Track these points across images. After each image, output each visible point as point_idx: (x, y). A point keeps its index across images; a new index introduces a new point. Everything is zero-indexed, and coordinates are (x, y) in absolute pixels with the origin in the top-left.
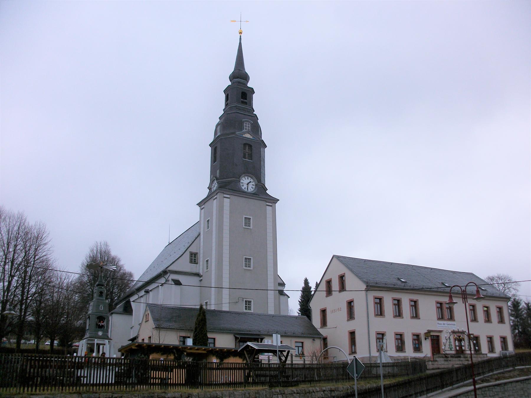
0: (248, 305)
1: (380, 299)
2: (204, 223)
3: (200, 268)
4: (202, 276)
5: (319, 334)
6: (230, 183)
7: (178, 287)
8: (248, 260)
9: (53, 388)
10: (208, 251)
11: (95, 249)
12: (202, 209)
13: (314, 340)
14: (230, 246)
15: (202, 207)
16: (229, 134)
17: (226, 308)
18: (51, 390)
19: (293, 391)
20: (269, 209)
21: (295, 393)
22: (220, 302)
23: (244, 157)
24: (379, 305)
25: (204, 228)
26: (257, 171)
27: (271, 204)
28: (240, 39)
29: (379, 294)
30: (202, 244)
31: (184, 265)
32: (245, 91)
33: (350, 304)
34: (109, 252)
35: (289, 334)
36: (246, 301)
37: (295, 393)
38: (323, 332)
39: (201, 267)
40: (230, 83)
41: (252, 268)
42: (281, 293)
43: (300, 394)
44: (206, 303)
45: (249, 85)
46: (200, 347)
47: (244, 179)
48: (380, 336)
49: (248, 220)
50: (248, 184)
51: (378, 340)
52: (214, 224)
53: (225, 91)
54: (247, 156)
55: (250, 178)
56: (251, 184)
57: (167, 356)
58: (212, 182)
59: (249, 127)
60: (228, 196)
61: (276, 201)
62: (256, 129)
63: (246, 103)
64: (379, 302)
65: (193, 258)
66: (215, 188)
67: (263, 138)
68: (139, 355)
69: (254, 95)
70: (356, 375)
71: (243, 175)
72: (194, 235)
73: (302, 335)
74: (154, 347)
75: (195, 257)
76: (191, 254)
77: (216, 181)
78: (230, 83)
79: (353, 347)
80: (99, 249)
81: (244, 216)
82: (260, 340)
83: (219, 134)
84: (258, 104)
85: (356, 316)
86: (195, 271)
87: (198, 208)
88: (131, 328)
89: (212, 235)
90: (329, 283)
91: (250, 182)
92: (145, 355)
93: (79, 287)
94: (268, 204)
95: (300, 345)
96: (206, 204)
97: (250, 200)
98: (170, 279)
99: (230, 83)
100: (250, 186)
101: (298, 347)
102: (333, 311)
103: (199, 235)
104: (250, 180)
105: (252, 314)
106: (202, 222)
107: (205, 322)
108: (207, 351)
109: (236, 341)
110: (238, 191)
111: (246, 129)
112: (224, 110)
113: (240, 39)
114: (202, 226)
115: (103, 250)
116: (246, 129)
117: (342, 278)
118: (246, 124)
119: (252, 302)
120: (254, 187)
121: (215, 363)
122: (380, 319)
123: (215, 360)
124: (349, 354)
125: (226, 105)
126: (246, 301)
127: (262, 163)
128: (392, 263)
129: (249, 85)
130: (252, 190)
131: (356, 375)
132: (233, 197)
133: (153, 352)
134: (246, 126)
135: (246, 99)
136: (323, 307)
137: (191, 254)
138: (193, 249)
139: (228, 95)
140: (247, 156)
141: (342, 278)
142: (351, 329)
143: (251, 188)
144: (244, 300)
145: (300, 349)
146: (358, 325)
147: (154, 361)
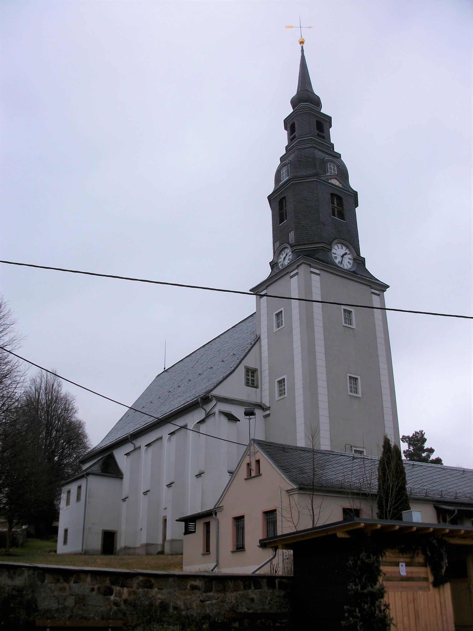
2: (269, 320)
3: (265, 393)
4: (269, 408)
6: (316, 250)
14: (327, 354)
23: (334, 215)
27: (377, 292)
28: (302, 51)
31: (235, 387)
32: (321, 121)
39: (266, 393)
41: (360, 395)
47: (336, 247)
50: (342, 257)
54: (336, 213)
55: (344, 248)
58: (277, 252)
60: (317, 271)
61: (384, 287)
62: (343, 174)
65: (250, 378)
66: (287, 262)
71: (336, 241)
75: (253, 376)
84: (340, 138)
91: (346, 254)
98: (216, 410)
103: (258, 339)
110: (328, 265)
112: (287, 148)
113: (302, 51)
120: (351, 262)
125: (291, 139)
130: (350, 266)
134: (331, 168)
138: (250, 362)
140: (336, 213)
144: (354, 449)
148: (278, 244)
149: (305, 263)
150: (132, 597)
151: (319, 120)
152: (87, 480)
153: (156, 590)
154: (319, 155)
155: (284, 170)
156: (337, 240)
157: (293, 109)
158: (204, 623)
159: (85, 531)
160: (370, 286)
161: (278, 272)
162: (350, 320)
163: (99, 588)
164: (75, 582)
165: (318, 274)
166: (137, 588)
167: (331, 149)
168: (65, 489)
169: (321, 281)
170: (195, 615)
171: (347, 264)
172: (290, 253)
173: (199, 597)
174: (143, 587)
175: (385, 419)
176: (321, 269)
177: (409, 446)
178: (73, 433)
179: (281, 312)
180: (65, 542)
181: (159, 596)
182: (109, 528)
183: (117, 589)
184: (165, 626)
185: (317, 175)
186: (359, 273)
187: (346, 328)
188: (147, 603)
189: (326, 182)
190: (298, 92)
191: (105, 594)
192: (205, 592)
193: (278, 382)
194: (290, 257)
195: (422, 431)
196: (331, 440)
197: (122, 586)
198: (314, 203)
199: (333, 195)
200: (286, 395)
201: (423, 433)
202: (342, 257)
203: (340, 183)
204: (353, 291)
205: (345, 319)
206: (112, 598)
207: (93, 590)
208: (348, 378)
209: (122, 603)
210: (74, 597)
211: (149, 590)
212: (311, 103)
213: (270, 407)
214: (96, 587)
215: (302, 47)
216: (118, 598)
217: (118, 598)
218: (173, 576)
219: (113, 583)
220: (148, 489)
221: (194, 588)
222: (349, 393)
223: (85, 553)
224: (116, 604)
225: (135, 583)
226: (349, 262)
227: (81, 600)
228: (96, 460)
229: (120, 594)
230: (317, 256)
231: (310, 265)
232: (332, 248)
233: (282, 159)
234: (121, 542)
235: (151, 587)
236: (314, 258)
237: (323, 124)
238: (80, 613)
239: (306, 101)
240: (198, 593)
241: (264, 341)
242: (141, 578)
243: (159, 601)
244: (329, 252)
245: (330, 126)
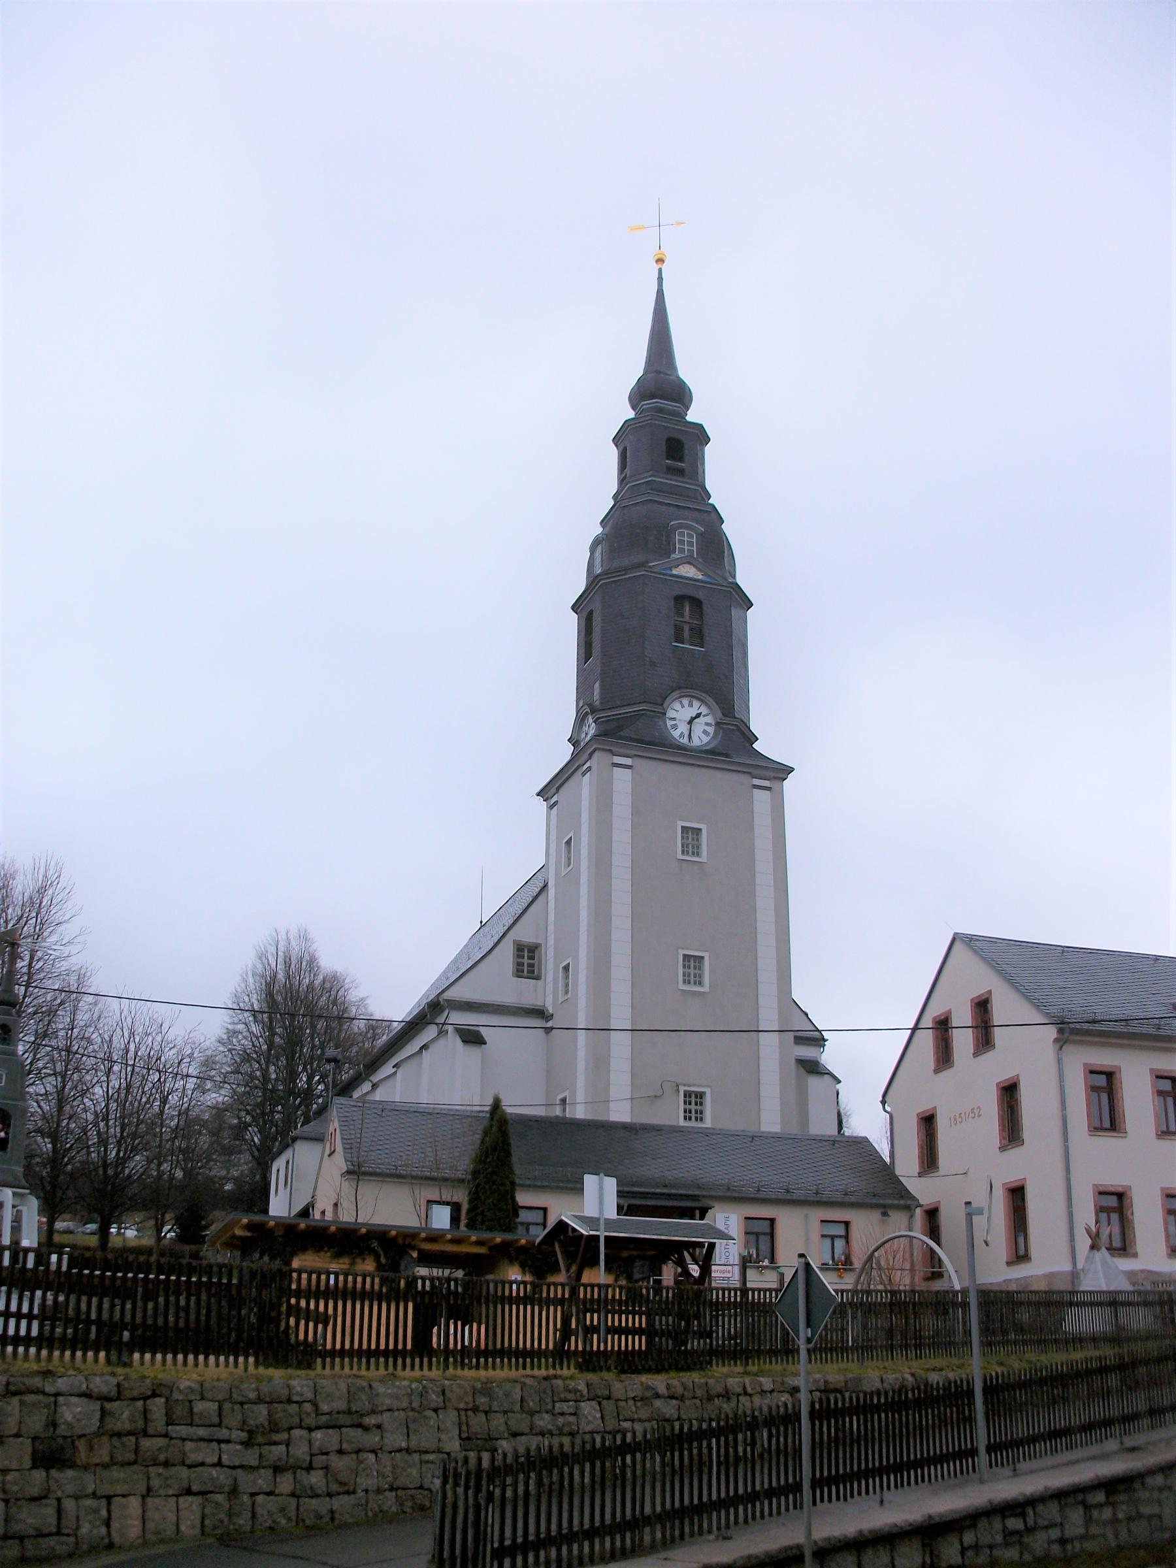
1: (1110, 1075)
3: (545, 993)
5: (904, 1193)
7: (474, 1052)
8: (693, 962)
9: (337, 1360)
10: (568, 940)
12: (551, 807)
13: (885, 1214)
15: (553, 801)
16: (626, 570)
17: (620, 1113)
18: (333, 1367)
19: (648, 1388)
20: (761, 798)
21: (658, 1396)
22: (600, 1096)
23: (679, 638)
24: (1104, 1096)
26: (719, 678)
29: (1104, 1058)
30: (551, 917)
31: (499, 983)
32: (679, 437)
33: (1009, 1091)
34: (312, 961)
35: (798, 1195)
36: (687, 1094)
37: (658, 1396)
38: (923, 1190)
39: (550, 989)
40: (631, 414)
41: (706, 988)
42: (813, 1068)
43: (682, 1398)
44: (564, 1101)
45: (692, 416)
46: (486, 1235)
47: (677, 705)
48: (1112, 1201)
49: (691, 834)
50: (690, 722)
51: (1104, 1216)
52: (584, 852)
53: (616, 440)
54: (686, 634)
55: (696, 704)
56: (701, 720)
57: (353, 1263)
58: (580, 720)
59: (690, 544)
60: (628, 761)
61: (783, 771)
62: (715, 548)
63: (681, 472)
64: (1105, 1085)
65: (526, 961)
67: (742, 580)
68: (257, 1255)
69: (708, 449)
70: (804, 1332)
71: (675, 694)
72: (536, 893)
73: (847, 1199)
74: (523, 1247)
75: (533, 958)
76: (520, 948)
77: (590, 719)
78: (631, 414)
79: (1021, 1240)
80: (282, 948)
81: (681, 823)
82: (697, 1213)
83: (598, 570)
84: (723, 476)
85: (1026, 1134)
86: (529, 1001)
87: (542, 805)
89: (578, 883)
90: (943, 1026)
91: (698, 715)
92: (273, 1258)
95: (840, 1230)
97: (696, 770)
100: (699, 727)
101: (833, 1237)
102: (957, 1120)
104: (696, 707)
105: (707, 1133)
108: (490, 1249)
111: (682, 550)
112: (615, 497)
116: (682, 550)
117: (982, 1006)
118: (682, 534)
120: (711, 730)
121: (519, 1283)
122: (1107, 1143)
123: (514, 1274)
124: (1009, 1264)
125: (622, 481)
126: (687, 1094)
127: (736, 654)
128: (1157, 958)
129: (692, 416)
130: (705, 739)
131: (804, 1332)
133: (304, 1250)
134: (682, 542)
135: (681, 459)
136: (924, 1107)
137: (520, 948)
138: (525, 933)
140: (686, 634)
141: (982, 1006)
142: (1013, 1177)
143: (702, 734)
144: (682, 1089)
145: (840, 1244)
146: (1033, 1162)
147: (310, 1274)
149: (603, 750)
165: (629, 767)
186: (735, 748)
190: (646, 372)
196: (633, 1076)
202: (690, 722)
203: (700, 570)
204: (713, 783)
208: (681, 958)
215: (660, 271)
222: (682, 986)
226: (705, 732)
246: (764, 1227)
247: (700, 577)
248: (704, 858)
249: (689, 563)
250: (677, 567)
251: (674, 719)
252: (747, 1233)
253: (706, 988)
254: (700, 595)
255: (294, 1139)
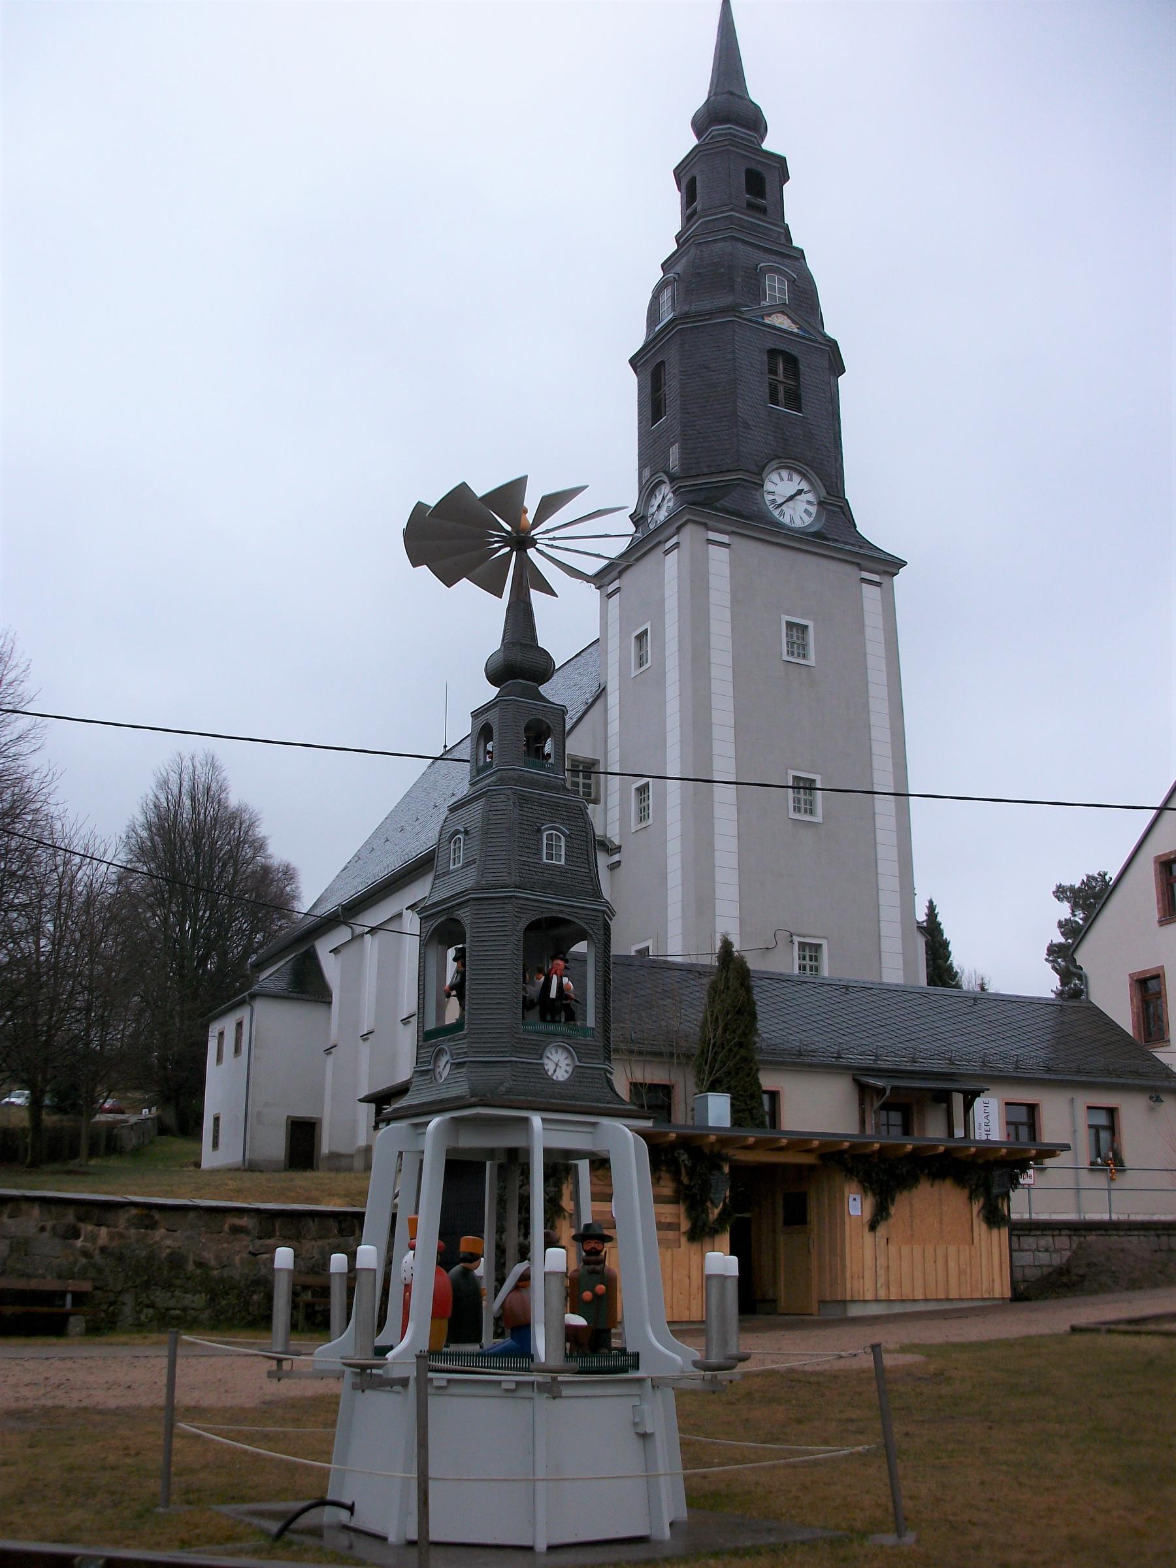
0: (807, 962)
2: (623, 648)
4: (618, 849)
6: (725, 489)
11: (174, 778)
12: (610, 596)
14: (740, 729)
23: (774, 399)
25: (623, 662)
27: (876, 578)
32: (760, 169)
34: (222, 788)
36: (802, 946)
40: (694, 141)
41: (818, 818)
45: (769, 144)
47: (774, 477)
54: (781, 396)
55: (796, 478)
58: (647, 491)
60: (724, 538)
61: (892, 565)
62: (805, 298)
63: (763, 210)
66: (662, 516)
71: (774, 464)
77: (666, 489)
81: (787, 618)
83: (667, 316)
84: (805, 212)
88: (328, 1051)
91: (800, 492)
93: (122, 908)
94: (865, 575)
96: (627, 576)
97: (801, 556)
99: (694, 141)
103: (602, 692)
106: (613, 644)
107: (753, 1016)
109: (862, 1101)
110: (753, 523)
114: (613, 657)
115: (202, 780)
119: (825, 949)
120: (813, 510)
125: (688, 218)
126: (802, 946)
129: (769, 144)
130: (808, 520)
132: (739, 543)
134: (772, 288)
135: (763, 196)
136: (1144, 965)
139: (693, 182)
140: (781, 396)
144: (796, 939)
148: (647, 473)
150: (115, 1244)
151: (753, 166)
152: (252, 1010)
153: (163, 1231)
154: (746, 255)
155: (666, 295)
156: (777, 461)
157: (699, 138)
158: (254, 1292)
159: (249, 1118)
160: (858, 565)
161: (647, 540)
162: (804, 647)
163: (54, 1228)
164: (10, 1217)
166: (127, 1228)
167: (783, 241)
168: (214, 1029)
169: (732, 563)
170: (237, 1277)
171: (800, 513)
172: (671, 495)
173: (247, 1246)
174: (138, 1227)
175: (880, 871)
176: (733, 533)
177: (1073, 911)
178: (266, 891)
179: (646, 631)
180: (215, 1145)
181: (168, 1242)
182: (303, 1112)
183: (87, 1228)
184: (177, 1293)
185: (732, 309)
186: (836, 536)
187: (791, 666)
188: (144, 1253)
189: (759, 323)
191: (65, 1238)
192: (260, 1238)
193: (638, 789)
194: (671, 504)
195: (1105, 874)
197: (99, 1225)
198: (739, 369)
199: (773, 353)
200: (650, 821)
201: (1107, 878)
203: (794, 322)
204: (820, 574)
205: (790, 644)
206: (79, 1243)
207: (43, 1229)
209: (97, 1251)
210: (8, 1242)
211: (150, 1232)
212: (737, 124)
213: (620, 847)
214: (49, 1225)
216: (89, 1245)
217: (89, 1245)
218: (196, 1208)
219: (80, 1219)
220: (370, 1029)
221: (236, 1230)
222: (792, 815)
223: (251, 1167)
224: (85, 1253)
225: (122, 1219)
226: (806, 511)
227: (20, 1246)
228: (282, 963)
229: (93, 1238)
230: (725, 503)
231: (705, 525)
232: (763, 481)
233: (666, 266)
234: (327, 1144)
235: (153, 1226)
236: (717, 510)
237: (763, 179)
238: (19, 1266)
239: (726, 120)
240: (246, 1240)
241: (613, 698)
242: (134, 1211)
243: (168, 1250)
244: (756, 490)
245: (785, 177)
246: (1022, 1115)
247: (796, 330)
248: (811, 661)
249: (783, 313)
250: (769, 315)
251: (772, 493)
252: (1008, 1123)
253: (818, 818)
254: (794, 351)
255: (253, 996)
